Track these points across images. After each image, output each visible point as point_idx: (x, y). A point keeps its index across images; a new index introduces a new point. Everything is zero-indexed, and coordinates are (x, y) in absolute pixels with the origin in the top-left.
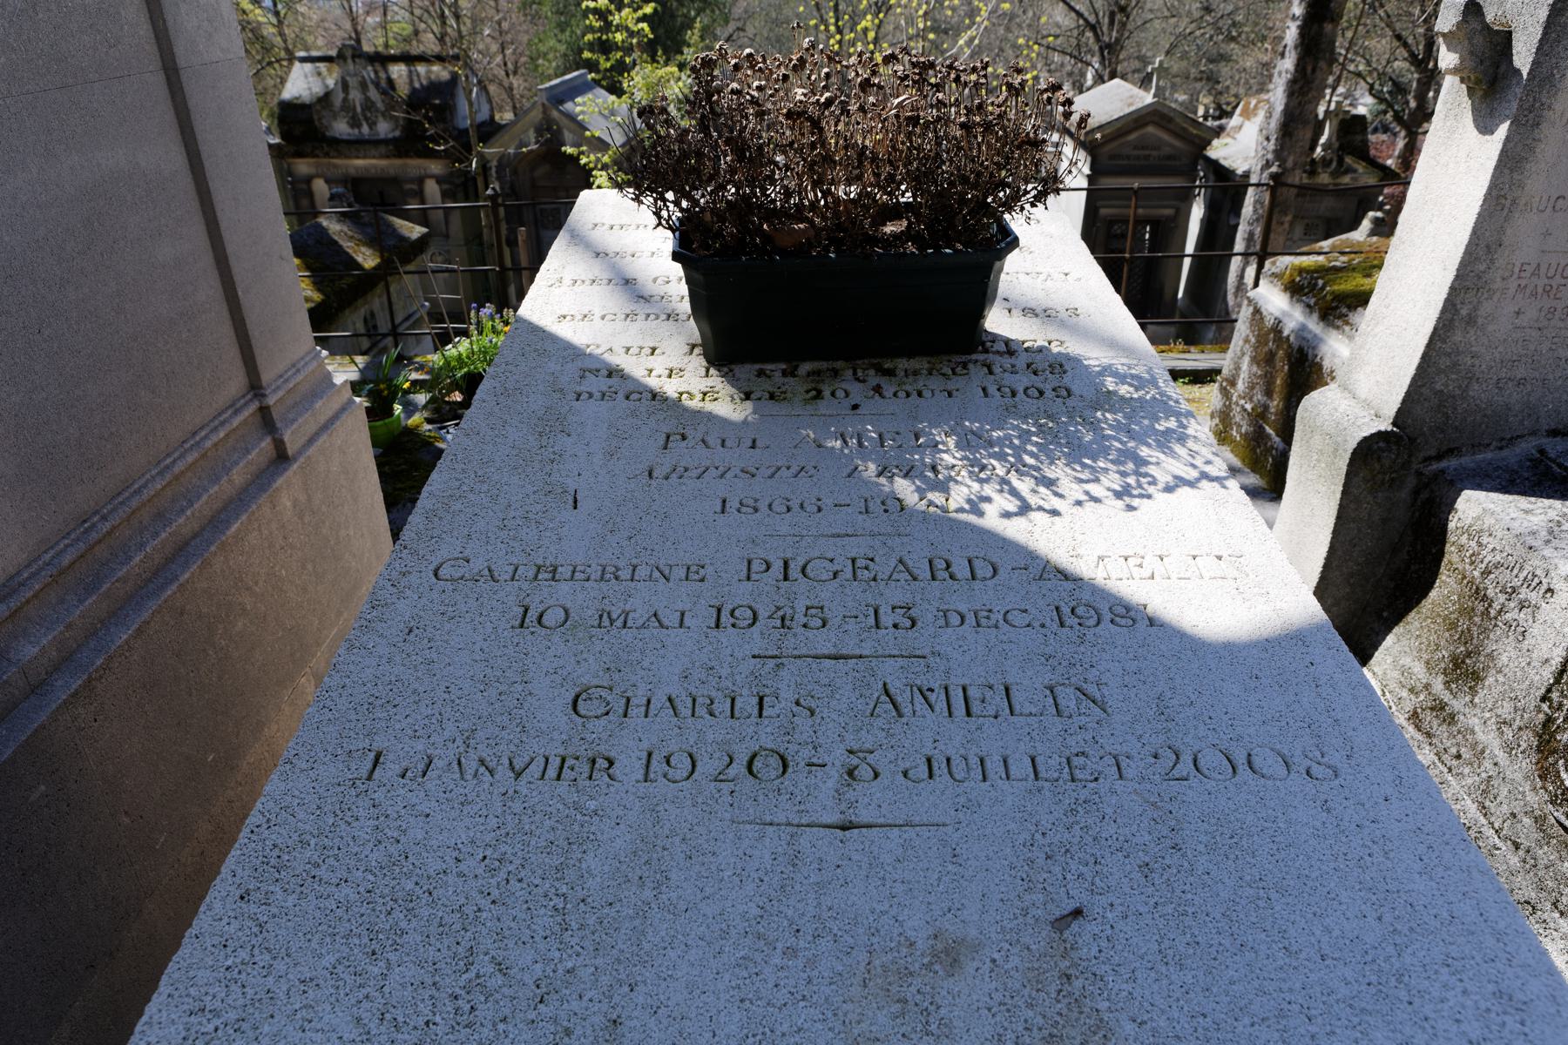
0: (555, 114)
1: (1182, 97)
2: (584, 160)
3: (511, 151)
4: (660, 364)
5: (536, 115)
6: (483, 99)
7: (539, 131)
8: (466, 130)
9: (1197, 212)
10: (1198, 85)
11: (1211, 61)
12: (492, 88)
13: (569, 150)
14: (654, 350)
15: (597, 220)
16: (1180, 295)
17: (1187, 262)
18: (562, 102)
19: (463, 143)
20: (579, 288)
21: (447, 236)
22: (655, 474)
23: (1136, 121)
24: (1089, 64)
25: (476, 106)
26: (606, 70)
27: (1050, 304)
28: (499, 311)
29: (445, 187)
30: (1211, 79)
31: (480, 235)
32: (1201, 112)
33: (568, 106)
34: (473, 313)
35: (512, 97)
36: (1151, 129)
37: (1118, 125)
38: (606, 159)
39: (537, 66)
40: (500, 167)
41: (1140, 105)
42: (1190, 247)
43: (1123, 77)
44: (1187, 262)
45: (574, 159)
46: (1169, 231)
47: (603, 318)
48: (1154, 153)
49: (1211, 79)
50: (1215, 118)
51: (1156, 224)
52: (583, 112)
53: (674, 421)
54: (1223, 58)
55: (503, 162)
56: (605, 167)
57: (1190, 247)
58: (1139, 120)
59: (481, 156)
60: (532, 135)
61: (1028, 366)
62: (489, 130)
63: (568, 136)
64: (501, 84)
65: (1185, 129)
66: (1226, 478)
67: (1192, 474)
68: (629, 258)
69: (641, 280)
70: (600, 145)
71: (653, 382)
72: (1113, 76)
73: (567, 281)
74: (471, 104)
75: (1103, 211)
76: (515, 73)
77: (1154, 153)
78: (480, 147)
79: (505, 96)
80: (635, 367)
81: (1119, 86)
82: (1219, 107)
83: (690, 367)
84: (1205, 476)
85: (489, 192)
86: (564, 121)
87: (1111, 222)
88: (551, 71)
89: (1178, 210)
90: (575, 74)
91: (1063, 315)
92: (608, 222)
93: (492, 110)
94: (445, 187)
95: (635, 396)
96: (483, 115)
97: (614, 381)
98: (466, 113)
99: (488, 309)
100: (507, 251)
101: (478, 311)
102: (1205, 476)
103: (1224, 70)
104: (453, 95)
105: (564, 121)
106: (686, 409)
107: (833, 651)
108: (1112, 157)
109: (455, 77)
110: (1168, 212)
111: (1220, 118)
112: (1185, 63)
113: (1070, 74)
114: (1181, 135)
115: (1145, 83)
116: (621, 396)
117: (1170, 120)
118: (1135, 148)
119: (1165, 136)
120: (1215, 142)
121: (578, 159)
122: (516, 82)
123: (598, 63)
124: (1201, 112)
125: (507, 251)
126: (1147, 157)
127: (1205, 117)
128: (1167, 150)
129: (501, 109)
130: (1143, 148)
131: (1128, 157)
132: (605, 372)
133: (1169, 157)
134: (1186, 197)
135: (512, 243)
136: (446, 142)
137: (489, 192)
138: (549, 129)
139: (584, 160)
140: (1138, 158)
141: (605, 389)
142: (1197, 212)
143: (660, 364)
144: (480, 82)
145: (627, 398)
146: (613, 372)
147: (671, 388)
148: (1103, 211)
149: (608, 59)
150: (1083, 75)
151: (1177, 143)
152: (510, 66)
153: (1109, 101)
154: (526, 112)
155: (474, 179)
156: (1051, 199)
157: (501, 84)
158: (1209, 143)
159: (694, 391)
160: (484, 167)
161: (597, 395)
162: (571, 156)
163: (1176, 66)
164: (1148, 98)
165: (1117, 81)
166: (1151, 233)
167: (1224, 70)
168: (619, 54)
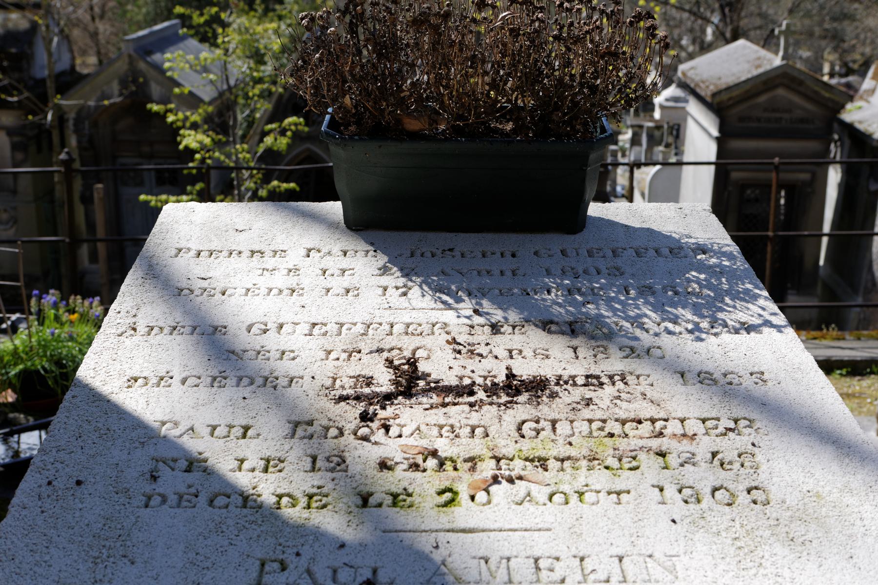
0: (142, 65)
1: (805, 54)
2: (171, 118)
3: (92, 103)
4: (253, 451)
5: (122, 66)
6: (64, 48)
7: (124, 84)
8: (43, 81)
9: (834, 176)
10: (823, 43)
11: (834, 19)
12: (76, 33)
13: (155, 108)
14: (246, 429)
15: (183, 244)
16: (822, 262)
18: (150, 53)
19: (40, 95)
20: (156, 339)
21: (14, 192)
23: (765, 83)
24: (708, 21)
25: (55, 57)
26: (199, 25)
27: (730, 367)
28: (65, 298)
29: (16, 139)
30: (837, 38)
31: (51, 192)
32: (826, 69)
33: (157, 57)
34: (33, 302)
35: (97, 44)
36: (781, 92)
37: (748, 87)
38: (195, 118)
39: (125, 12)
40: (78, 121)
41: (768, 67)
43: (748, 38)
45: (162, 117)
46: (807, 195)
47: (184, 381)
48: (786, 116)
49: (837, 38)
50: (842, 76)
51: (792, 189)
52: (170, 69)
53: (272, 540)
54: (846, 16)
55: (82, 114)
56: (195, 126)
58: (767, 82)
59: (58, 108)
60: (115, 87)
61: (714, 454)
62: (69, 80)
63: (155, 90)
64: (85, 29)
65: (816, 92)
66: (785, 327)
67: (757, 321)
68: (218, 296)
69: (231, 329)
70: (192, 101)
71: (243, 480)
72: (735, 37)
73: (142, 329)
74: (50, 54)
75: (735, 175)
76: (102, 17)
77: (786, 116)
78: (58, 100)
79: (88, 41)
80: (221, 457)
81: (744, 47)
82: (845, 64)
83: (292, 457)
84: (767, 323)
85: (63, 156)
86: (152, 73)
87: (743, 186)
88: (140, 18)
89: (814, 174)
90: (166, 24)
91: (748, 382)
92: (195, 246)
93: (73, 59)
94: (16, 139)
95: (221, 501)
96: (63, 64)
97: (193, 477)
98: (42, 65)
99: (52, 296)
100: (80, 210)
101: (40, 298)
102: (767, 323)
103: (848, 28)
104: (31, 44)
105: (152, 73)
106: (285, 523)
108: (742, 119)
109: (34, 27)
110: (805, 176)
111: (846, 75)
112: (807, 22)
113: (691, 30)
114: (813, 97)
115: (768, 41)
116: (203, 499)
117: (801, 83)
119: (796, 99)
120: (849, 106)
121: (164, 117)
122: (103, 28)
123: (190, 17)
124: (826, 69)
125: (80, 210)
127: (832, 75)
129: (84, 53)
130: (774, 110)
131: (759, 120)
132: (183, 464)
133: (802, 121)
134: (824, 166)
135: (87, 199)
136: (20, 93)
137: (63, 156)
138: (135, 81)
139: (171, 118)
141: (182, 489)
142: (834, 176)
143: (253, 451)
144: (62, 31)
145: (211, 502)
146: (194, 465)
147: (266, 489)
148: (735, 175)
149: (202, 15)
150: (703, 32)
151: (809, 106)
152: (97, 10)
153: (736, 62)
154: (112, 62)
155: (49, 133)
157: (85, 29)
158: (843, 107)
159: (298, 494)
160: (61, 119)
161: (173, 499)
162: (157, 114)
163: (798, 26)
164: (777, 61)
165: (741, 42)
167: (848, 28)
168: (214, 10)
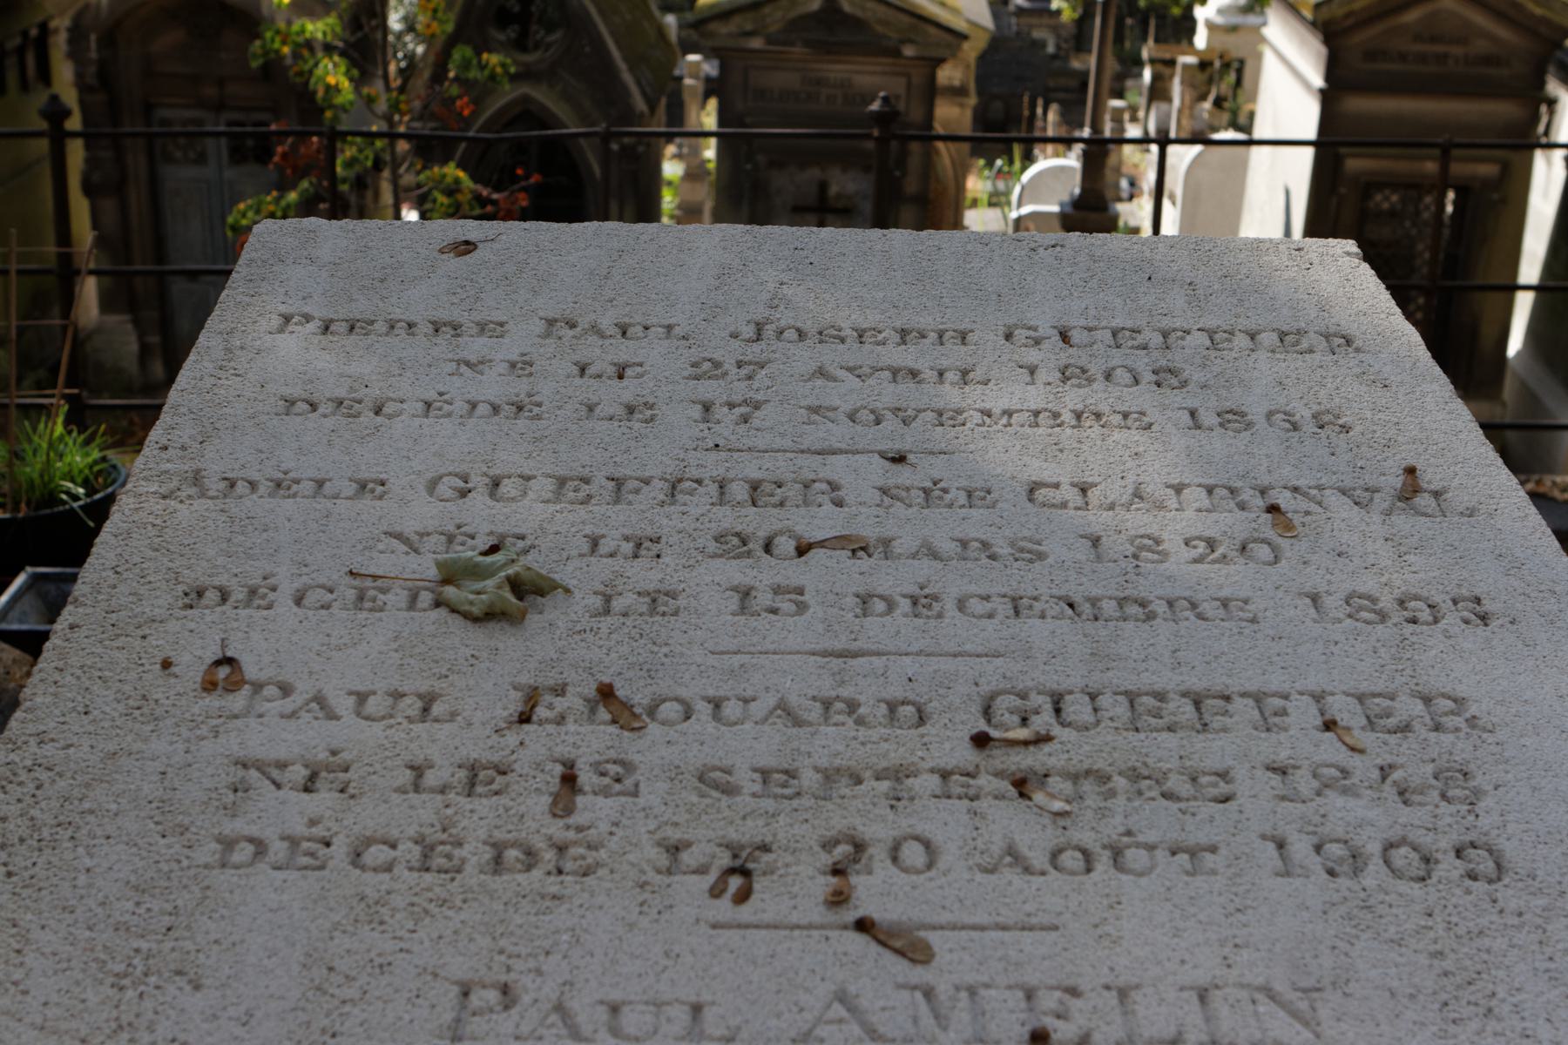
17: (1524, 305)
22: (305, 602)
42: (1530, 269)
44: (1524, 305)
48: (1457, 51)
57: (1530, 269)
77: (1457, 51)
87: (1369, 186)
89: (1506, 167)
107: (748, 932)
108: (1371, 55)
110: (1487, 170)
118: (1418, 38)
126: (1442, 58)
128: (1480, 46)
130: (1434, 39)
131: (1403, 57)
133: (1488, 60)
140: (1422, 58)
151: (1503, 32)
156: (1043, 732)
161: (239, 594)
166: (1455, 203)
